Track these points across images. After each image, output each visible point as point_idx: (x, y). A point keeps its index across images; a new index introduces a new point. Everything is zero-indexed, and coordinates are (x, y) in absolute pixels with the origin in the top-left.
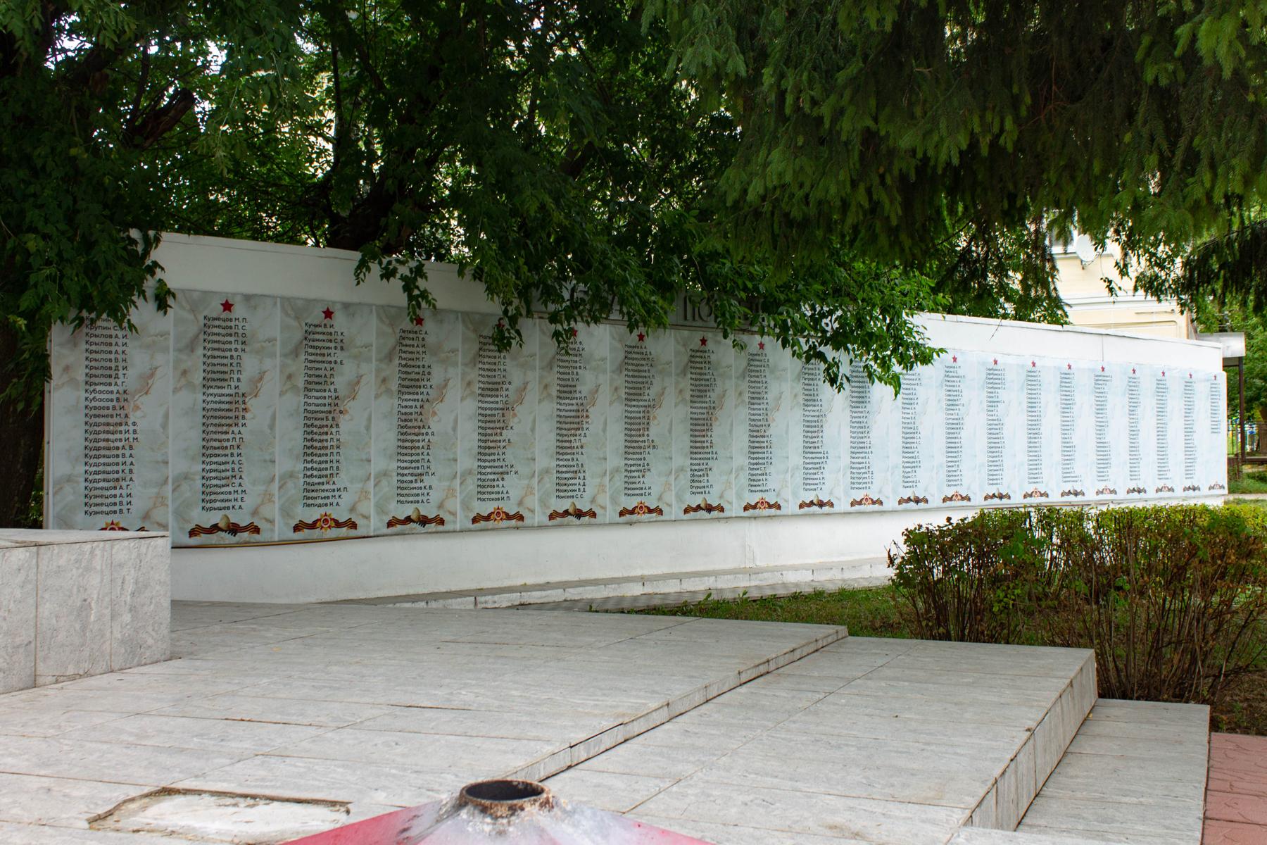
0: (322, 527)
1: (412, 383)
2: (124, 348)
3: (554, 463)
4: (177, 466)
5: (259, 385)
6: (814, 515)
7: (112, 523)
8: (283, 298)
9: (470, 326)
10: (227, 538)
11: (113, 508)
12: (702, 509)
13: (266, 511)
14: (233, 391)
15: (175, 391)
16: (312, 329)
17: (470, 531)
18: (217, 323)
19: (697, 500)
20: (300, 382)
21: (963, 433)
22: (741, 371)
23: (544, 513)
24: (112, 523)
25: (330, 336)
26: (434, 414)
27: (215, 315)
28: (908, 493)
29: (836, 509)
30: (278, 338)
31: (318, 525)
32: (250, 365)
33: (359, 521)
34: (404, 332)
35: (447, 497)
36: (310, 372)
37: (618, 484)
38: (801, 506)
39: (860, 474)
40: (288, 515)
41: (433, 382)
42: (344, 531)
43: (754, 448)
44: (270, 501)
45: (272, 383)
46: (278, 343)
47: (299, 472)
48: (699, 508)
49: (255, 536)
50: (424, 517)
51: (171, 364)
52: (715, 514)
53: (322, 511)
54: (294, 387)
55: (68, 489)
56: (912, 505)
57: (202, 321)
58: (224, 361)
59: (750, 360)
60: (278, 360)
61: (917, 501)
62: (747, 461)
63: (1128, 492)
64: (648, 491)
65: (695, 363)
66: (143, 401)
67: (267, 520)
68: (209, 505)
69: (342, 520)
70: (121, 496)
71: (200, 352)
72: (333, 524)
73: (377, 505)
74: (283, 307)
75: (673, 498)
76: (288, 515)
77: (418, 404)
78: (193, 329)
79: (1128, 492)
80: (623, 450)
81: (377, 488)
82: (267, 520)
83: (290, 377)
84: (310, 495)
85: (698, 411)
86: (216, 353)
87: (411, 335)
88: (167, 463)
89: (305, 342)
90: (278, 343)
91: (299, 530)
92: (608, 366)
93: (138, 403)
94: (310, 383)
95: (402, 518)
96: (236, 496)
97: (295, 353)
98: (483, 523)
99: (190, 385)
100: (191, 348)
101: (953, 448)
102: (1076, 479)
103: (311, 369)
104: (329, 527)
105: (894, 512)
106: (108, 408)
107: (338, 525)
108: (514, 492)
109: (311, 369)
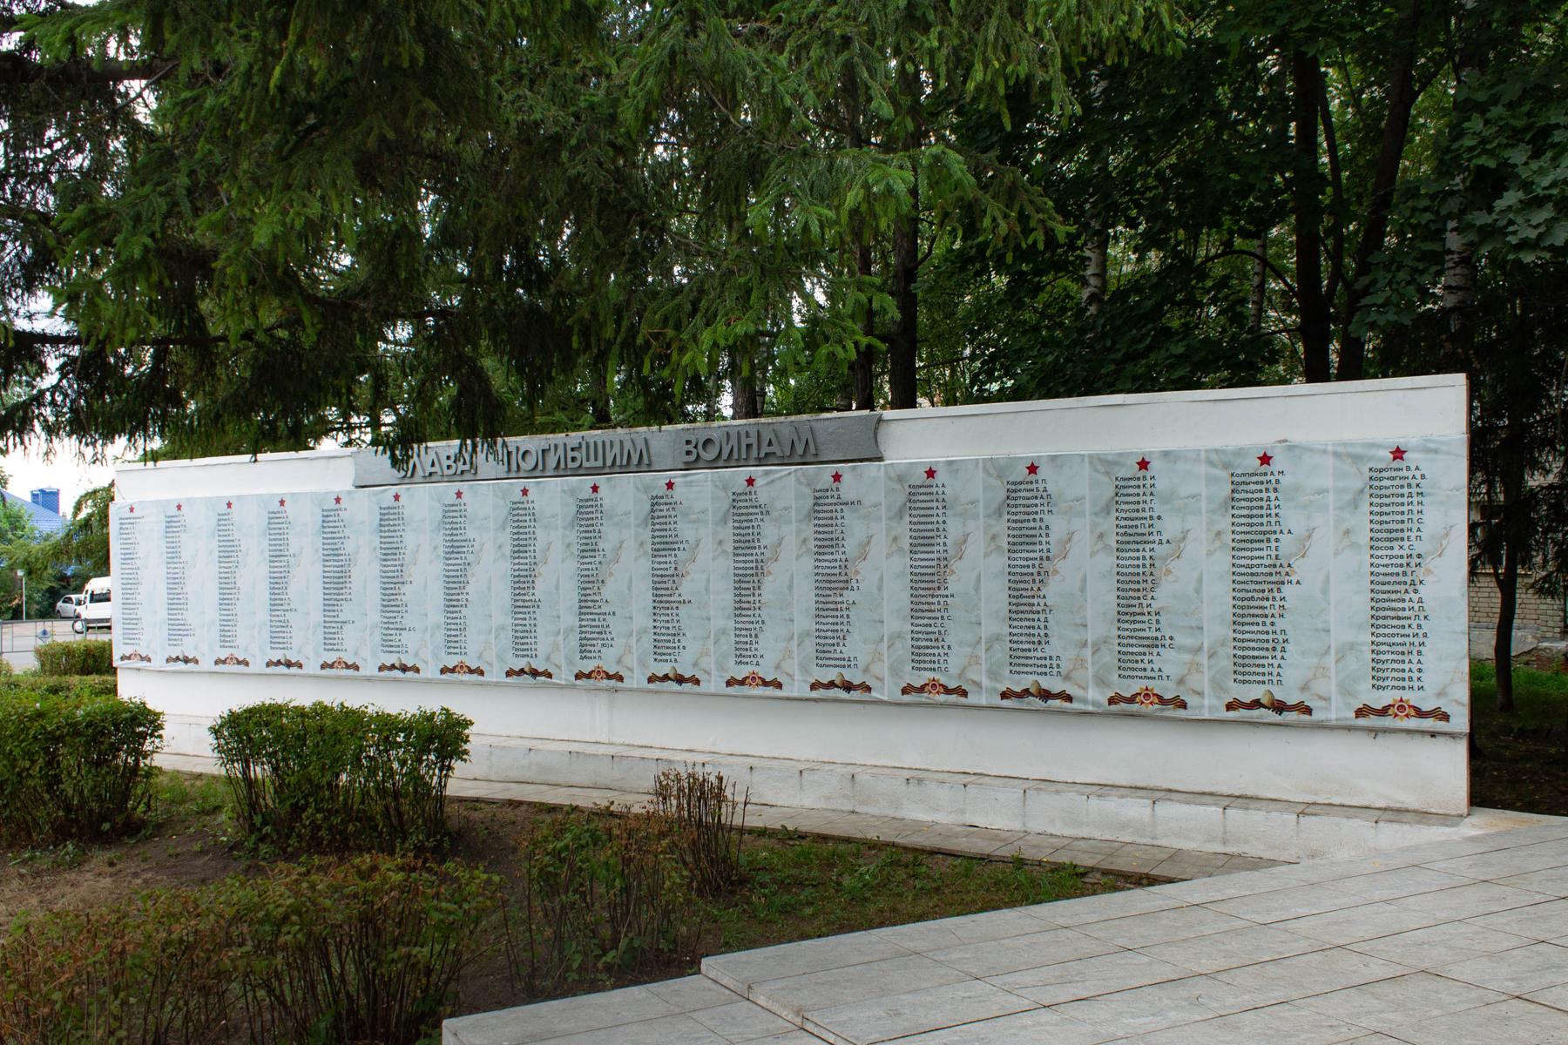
0: (1396, 715)
1: (1028, 540)
2: (1277, 511)
3: (443, 620)
4: (1340, 635)
5: (1444, 542)
6: (395, 680)
7: (1401, 700)
8: (1090, 456)
9: (1099, 467)
10: (1270, 716)
11: (1043, 670)
12: (837, 686)
13: (1194, 681)
14: (1405, 552)
15: (986, 555)
16: (1123, 483)
17: (1349, 729)
18: (922, 490)
19: (663, 669)
20: (906, 543)
21: (469, 588)
22: (720, 515)
23: (643, 674)
24: (1401, 700)
25: (673, 505)
26: (1169, 572)
27: (919, 483)
28: (391, 659)
29: (362, 672)
30: (1204, 494)
31: (1390, 712)
32: (954, 528)
33: (1191, 700)
34: (914, 487)
35: (873, 661)
36: (914, 534)
37: (1107, 659)
38: (380, 669)
39: (926, 647)
40: (1221, 688)
41: (763, 542)
42: (953, 698)
43: (1378, 609)
44: (707, 654)
45: (880, 546)
46: (981, 505)
47: (1363, 644)
48: (666, 678)
49: (1443, 723)
50: (681, 676)
51: (1088, 527)
52: (856, 695)
53: (931, 675)
54: (1106, 547)
55: (997, 647)
56: (282, 669)
57: (1368, 474)
58: (930, 527)
59: (653, 505)
60: (1088, 519)
61: (289, 664)
62: (511, 621)
63: (168, 661)
64: (534, 653)
65: (740, 508)
66: (861, 566)
67: (1321, 698)
68: (917, 665)
69: (1167, 696)
70: (1410, 670)
71: (1366, 508)
72: (1413, 713)
73: (567, 657)
74: (1091, 463)
75: (886, 671)
76: (1221, 688)
77: (1037, 563)
78: (1357, 484)
79: (168, 661)
80: (650, 610)
81: (1096, 657)
82: (1321, 698)
83: (994, 538)
84: (919, 658)
85: (1128, 563)
86: (923, 519)
87: (744, 497)
88: (1202, 628)
89: (908, 505)
90: (981, 505)
91: (1234, 709)
92: (632, 520)
93: (1170, 567)
94: (915, 545)
95: (825, 681)
96: (1270, 669)
97: (900, 515)
98: (1123, 706)
99: (1354, 545)
100: (900, 515)
101: (454, 601)
102: (1048, 665)
103: (915, 531)
104: (1407, 716)
105: (497, 685)
106: (1398, 574)
107: (948, 691)
108: (769, 656)
109: (915, 531)
